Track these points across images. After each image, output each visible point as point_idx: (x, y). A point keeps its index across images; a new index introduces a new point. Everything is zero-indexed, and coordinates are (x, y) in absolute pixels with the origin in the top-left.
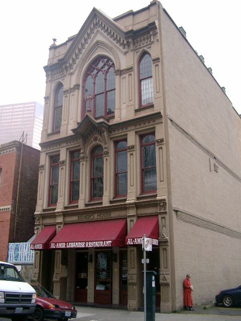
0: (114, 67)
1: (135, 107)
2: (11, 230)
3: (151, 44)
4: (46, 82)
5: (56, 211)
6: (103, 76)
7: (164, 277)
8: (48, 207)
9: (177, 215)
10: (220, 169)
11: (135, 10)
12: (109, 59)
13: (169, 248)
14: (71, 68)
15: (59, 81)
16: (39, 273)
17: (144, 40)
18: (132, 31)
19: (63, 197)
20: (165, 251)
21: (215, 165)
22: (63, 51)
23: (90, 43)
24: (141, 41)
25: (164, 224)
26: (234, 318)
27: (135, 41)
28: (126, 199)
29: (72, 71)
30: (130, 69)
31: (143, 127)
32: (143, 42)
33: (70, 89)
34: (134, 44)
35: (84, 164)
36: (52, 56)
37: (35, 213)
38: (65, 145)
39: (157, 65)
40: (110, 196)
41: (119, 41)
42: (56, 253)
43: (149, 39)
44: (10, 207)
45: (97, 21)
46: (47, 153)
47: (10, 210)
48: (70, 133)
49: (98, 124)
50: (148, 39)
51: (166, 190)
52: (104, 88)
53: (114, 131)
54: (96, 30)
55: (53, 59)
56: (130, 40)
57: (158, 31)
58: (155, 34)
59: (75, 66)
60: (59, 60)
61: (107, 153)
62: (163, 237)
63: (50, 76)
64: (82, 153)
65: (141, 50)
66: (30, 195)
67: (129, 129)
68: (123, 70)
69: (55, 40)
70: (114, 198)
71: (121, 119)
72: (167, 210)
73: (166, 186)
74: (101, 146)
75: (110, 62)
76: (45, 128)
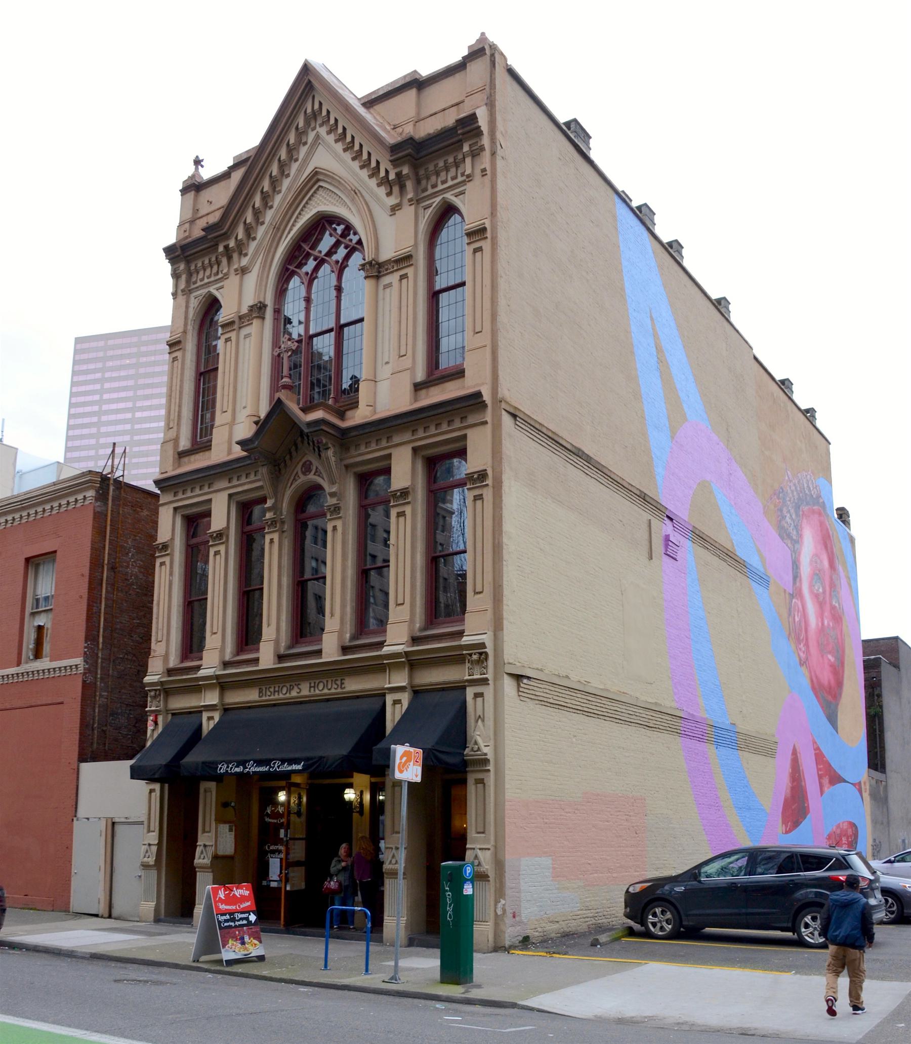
0: (362, 250)
2: (85, 725)
3: (463, 183)
4: (175, 295)
5: (202, 673)
7: (476, 857)
8: (182, 661)
9: (519, 686)
10: (688, 550)
11: (425, 71)
13: (491, 779)
14: (241, 248)
15: (209, 291)
16: (159, 844)
17: (447, 169)
18: (410, 141)
19: (219, 635)
21: (667, 539)
22: (221, 196)
23: (296, 175)
24: (438, 174)
25: (479, 712)
27: (422, 172)
28: (201, 665)
30: (405, 260)
32: (443, 175)
33: (240, 318)
34: (418, 182)
35: (276, 540)
36: (189, 215)
37: (147, 679)
39: (480, 249)
40: (412, 621)
41: (375, 173)
44: (79, 661)
45: (316, 106)
46: (175, 509)
47: (81, 670)
48: (238, 452)
49: (309, 424)
51: (489, 615)
52: (333, 317)
53: (357, 446)
54: (311, 136)
55: (192, 222)
56: (405, 170)
57: (486, 141)
58: (476, 153)
60: (208, 229)
61: (336, 509)
63: (184, 277)
64: (269, 509)
65: (438, 199)
67: (397, 439)
68: (389, 261)
69: (198, 162)
70: (353, 638)
71: (375, 412)
72: (490, 676)
73: (489, 606)
74: (319, 487)
75: (351, 236)
76: (172, 434)
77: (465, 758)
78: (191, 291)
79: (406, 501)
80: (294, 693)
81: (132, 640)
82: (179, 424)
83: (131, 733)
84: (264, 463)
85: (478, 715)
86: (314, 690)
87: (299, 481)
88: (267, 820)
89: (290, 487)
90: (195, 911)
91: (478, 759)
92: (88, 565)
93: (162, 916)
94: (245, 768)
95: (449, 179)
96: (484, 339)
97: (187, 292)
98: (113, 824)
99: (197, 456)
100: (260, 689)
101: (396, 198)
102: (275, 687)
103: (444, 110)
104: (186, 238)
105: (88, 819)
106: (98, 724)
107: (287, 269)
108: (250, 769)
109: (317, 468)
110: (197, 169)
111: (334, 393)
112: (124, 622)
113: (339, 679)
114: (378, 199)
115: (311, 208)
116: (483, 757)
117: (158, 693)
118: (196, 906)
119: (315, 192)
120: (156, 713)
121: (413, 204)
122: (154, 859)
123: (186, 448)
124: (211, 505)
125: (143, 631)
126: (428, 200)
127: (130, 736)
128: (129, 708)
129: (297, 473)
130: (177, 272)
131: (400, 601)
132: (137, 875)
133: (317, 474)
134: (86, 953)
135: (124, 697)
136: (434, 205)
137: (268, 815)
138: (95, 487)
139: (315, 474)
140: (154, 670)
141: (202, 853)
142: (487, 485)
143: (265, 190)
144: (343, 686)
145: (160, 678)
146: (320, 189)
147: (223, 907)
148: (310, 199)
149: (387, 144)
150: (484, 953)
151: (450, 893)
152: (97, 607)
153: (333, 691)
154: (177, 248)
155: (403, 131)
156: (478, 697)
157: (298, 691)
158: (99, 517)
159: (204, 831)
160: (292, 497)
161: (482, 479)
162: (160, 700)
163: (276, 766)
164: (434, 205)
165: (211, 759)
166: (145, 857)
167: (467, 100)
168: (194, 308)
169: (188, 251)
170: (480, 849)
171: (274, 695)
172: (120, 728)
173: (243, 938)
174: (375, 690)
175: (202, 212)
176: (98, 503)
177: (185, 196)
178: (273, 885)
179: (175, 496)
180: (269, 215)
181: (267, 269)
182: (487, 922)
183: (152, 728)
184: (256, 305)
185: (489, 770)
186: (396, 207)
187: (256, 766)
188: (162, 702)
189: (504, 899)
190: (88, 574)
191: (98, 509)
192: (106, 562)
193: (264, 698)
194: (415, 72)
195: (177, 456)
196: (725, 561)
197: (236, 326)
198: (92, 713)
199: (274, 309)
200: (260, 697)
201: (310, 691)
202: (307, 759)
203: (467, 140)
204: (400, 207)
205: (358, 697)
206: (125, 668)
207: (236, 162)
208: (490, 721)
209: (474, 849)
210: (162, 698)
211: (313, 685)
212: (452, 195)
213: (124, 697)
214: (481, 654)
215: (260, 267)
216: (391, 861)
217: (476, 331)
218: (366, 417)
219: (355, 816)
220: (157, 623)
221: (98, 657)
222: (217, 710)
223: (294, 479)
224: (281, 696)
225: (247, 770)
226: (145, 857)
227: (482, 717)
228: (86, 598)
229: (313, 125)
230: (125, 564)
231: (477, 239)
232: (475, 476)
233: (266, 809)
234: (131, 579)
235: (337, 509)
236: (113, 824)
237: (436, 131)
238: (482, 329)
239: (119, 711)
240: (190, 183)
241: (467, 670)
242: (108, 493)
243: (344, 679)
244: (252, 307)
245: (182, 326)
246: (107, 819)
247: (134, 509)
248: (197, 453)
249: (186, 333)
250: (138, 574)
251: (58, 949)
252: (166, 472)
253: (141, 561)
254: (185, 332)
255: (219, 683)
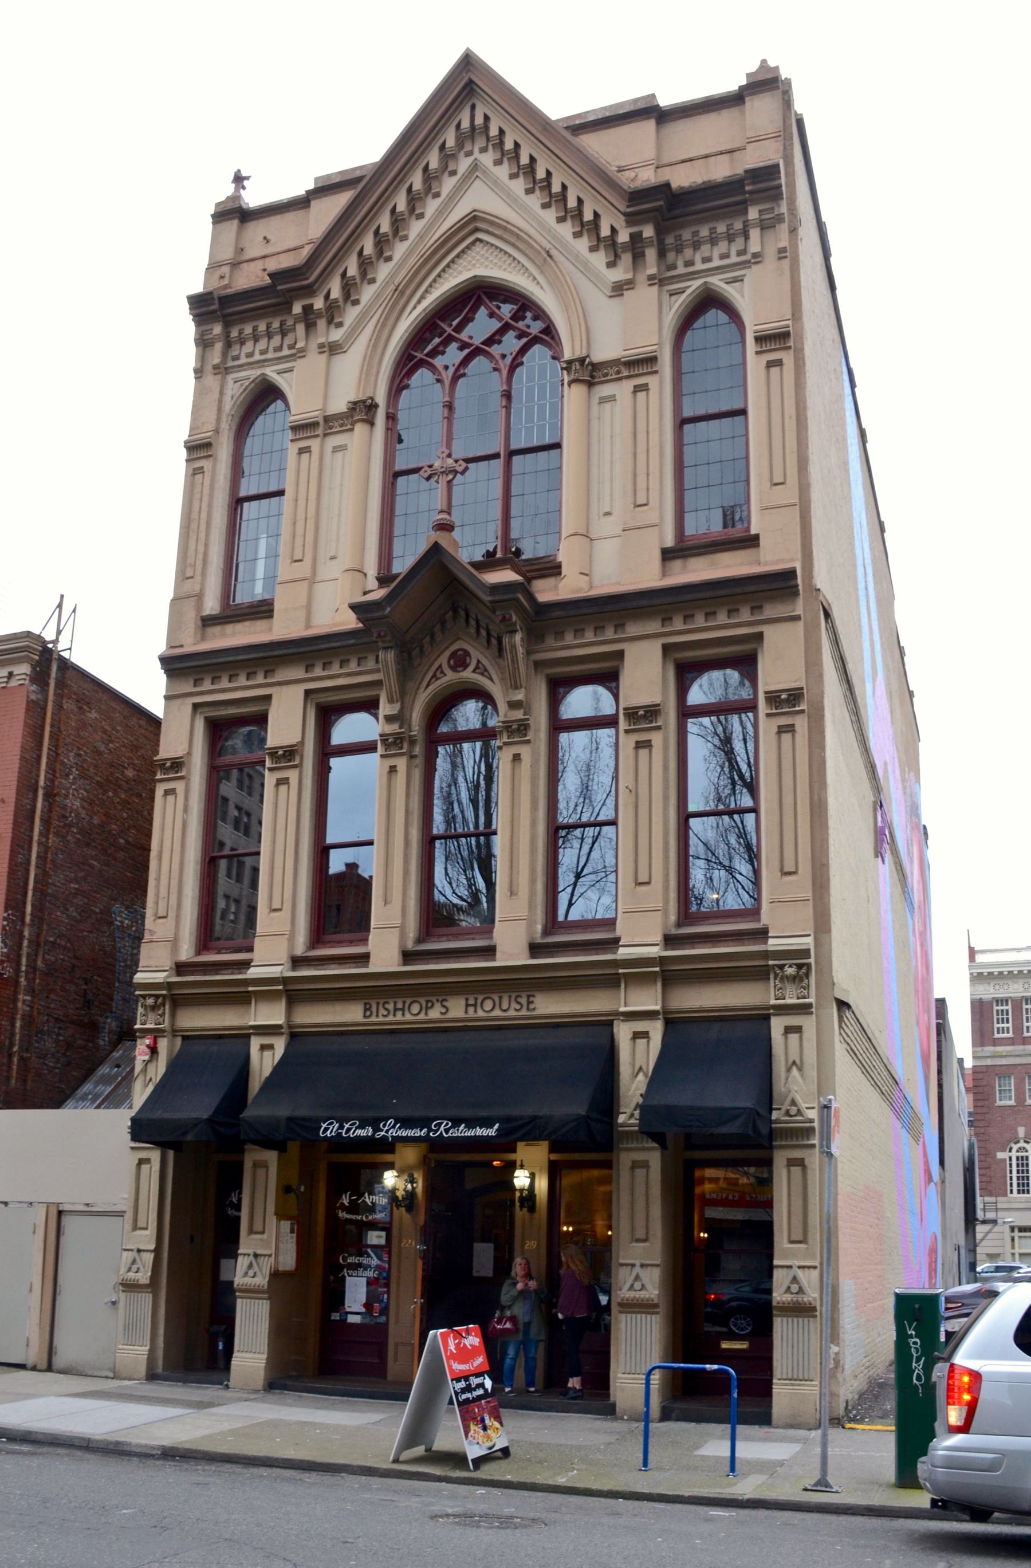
1: (662, 538)
3: (746, 265)
6: (496, 383)
7: (795, 1280)
8: (198, 952)
11: (665, 101)
12: (525, 305)
13: (814, 1159)
14: (332, 313)
16: (157, 1251)
17: (713, 241)
20: (796, 1170)
25: (794, 1055)
26: (153, 1407)
27: (670, 240)
28: (251, 960)
29: (336, 335)
31: (338, 676)
33: (327, 419)
34: (662, 254)
37: (139, 977)
38: (297, 672)
42: (248, 1165)
43: (740, 241)
45: (479, 120)
46: (196, 707)
48: (350, 621)
50: (730, 238)
53: (559, 635)
54: (463, 164)
56: (648, 231)
59: (351, 315)
62: (793, 1110)
63: (219, 346)
65: (696, 284)
66: (78, 893)
67: (633, 629)
69: (239, 179)
75: (528, 321)
77: (773, 1125)
78: (227, 371)
79: (654, 725)
80: (435, 1013)
81: (68, 915)
82: (204, 574)
83: (59, 1066)
84: (390, 645)
85: (637, 1068)
86: (475, 1011)
87: (445, 679)
88: (343, 1215)
89: (428, 685)
90: (232, 1362)
91: (789, 1127)
92: (14, 785)
93: (160, 1370)
94: (377, 1129)
95: (271, 349)
96: (789, 494)
97: (222, 370)
98: (60, 1213)
99: (229, 628)
100: (366, 1004)
101: (625, 272)
102: (395, 1003)
103: (706, 157)
104: (226, 287)
105: (6, 1204)
106: (20, 1048)
107: (411, 357)
108: (387, 1131)
109: (479, 662)
110: (237, 189)
111: (502, 551)
112: (59, 884)
113: (524, 995)
114: (586, 269)
115: (460, 269)
116: (808, 1125)
117: (160, 1001)
118: (235, 1355)
119: (468, 247)
120: (156, 1034)
121: (655, 284)
122: (149, 1274)
123: (214, 613)
124: (270, 704)
125: (81, 903)
126: (678, 282)
127: (57, 1071)
128: (57, 1025)
129: (440, 666)
130: (206, 337)
131: (276, 905)
132: (108, 1299)
133: (477, 671)
134: (153, 1448)
135: (52, 1006)
136: (689, 291)
137: (343, 1208)
138: (33, 659)
139: (474, 671)
140: (152, 963)
141: (250, 1266)
142: (802, 711)
143: (381, 231)
144: (532, 1006)
145: (167, 977)
146: (478, 243)
147: (458, 1367)
148: (458, 256)
149: (626, 188)
150: (810, 1429)
151: (918, 1340)
152: (24, 855)
153: (512, 1013)
154: (213, 299)
155: (636, 176)
156: (791, 1033)
157: (444, 1010)
158: (35, 709)
159: (251, 1231)
160: (428, 704)
161: (524, 732)
162: (164, 1013)
163: (442, 1128)
164: (689, 291)
165: (302, 1112)
166: (129, 1270)
167: (749, 147)
168: (232, 397)
169: (231, 307)
170: (799, 1267)
171: (394, 1015)
172: (46, 1055)
173: (483, 1420)
174: (712, 1011)
175: (250, 254)
176: (34, 688)
177: (218, 226)
178: (352, 1319)
179: (195, 686)
180: (383, 271)
181: (379, 351)
182: (812, 1380)
183: (147, 1058)
184: (364, 401)
185: (813, 1146)
186: (626, 284)
187: (400, 1128)
188: (167, 1016)
189: (838, 1345)
190: (14, 800)
191: (33, 697)
192: (42, 783)
193: (374, 1019)
194: (653, 96)
195: (199, 623)
196: (898, 873)
197: (320, 431)
198: (9, 1028)
199: (387, 413)
200: (365, 1016)
201: (466, 1012)
202: (504, 1120)
203: (755, 202)
204: (632, 286)
205: (220, 1037)
206: (56, 960)
207: (320, 185)
208: (811, 1071)
209: (790, 1267)
210: (167, 1011)
211: (471, 1002)
212: (721, 280)
213: (52, 1006)
214: (800, 966)
215: (368, 346)
216: (632, 1286)
217: (295, 559)
218: (580, 590)
219: (520, 1214)
220: (158, 886)
221: (21, 936)
222: (282, 1034)
223: (434, 676)
224: (408, 1017)
225: (383, 1133)
226: (129, 1270)
227: (798, 1062)
228: (9, 839)
229: (468, 147)
230: (63, 791)
231: (778, 346)
232: (281, 752)
233: (230, 1196)
234: (70, 816)
235: (522, 728)
236: (60, 1213)
237: (694, 185)
238: (303, 556)
239: (46, 1028)
240: (229, 206)
241: (772, 990)
242: (49, 676)
243: (533, 996)
244: (355, 403)
245: (214, 422)
246: (48, 1205)
247: (80, 705)
248: (239, 621)
249: (218, 433)
250: (80, 810)
251: (83, 1439)
252: (182, 646)
253: (85, 790)
254: (217, 431)
255: (287, 991)
